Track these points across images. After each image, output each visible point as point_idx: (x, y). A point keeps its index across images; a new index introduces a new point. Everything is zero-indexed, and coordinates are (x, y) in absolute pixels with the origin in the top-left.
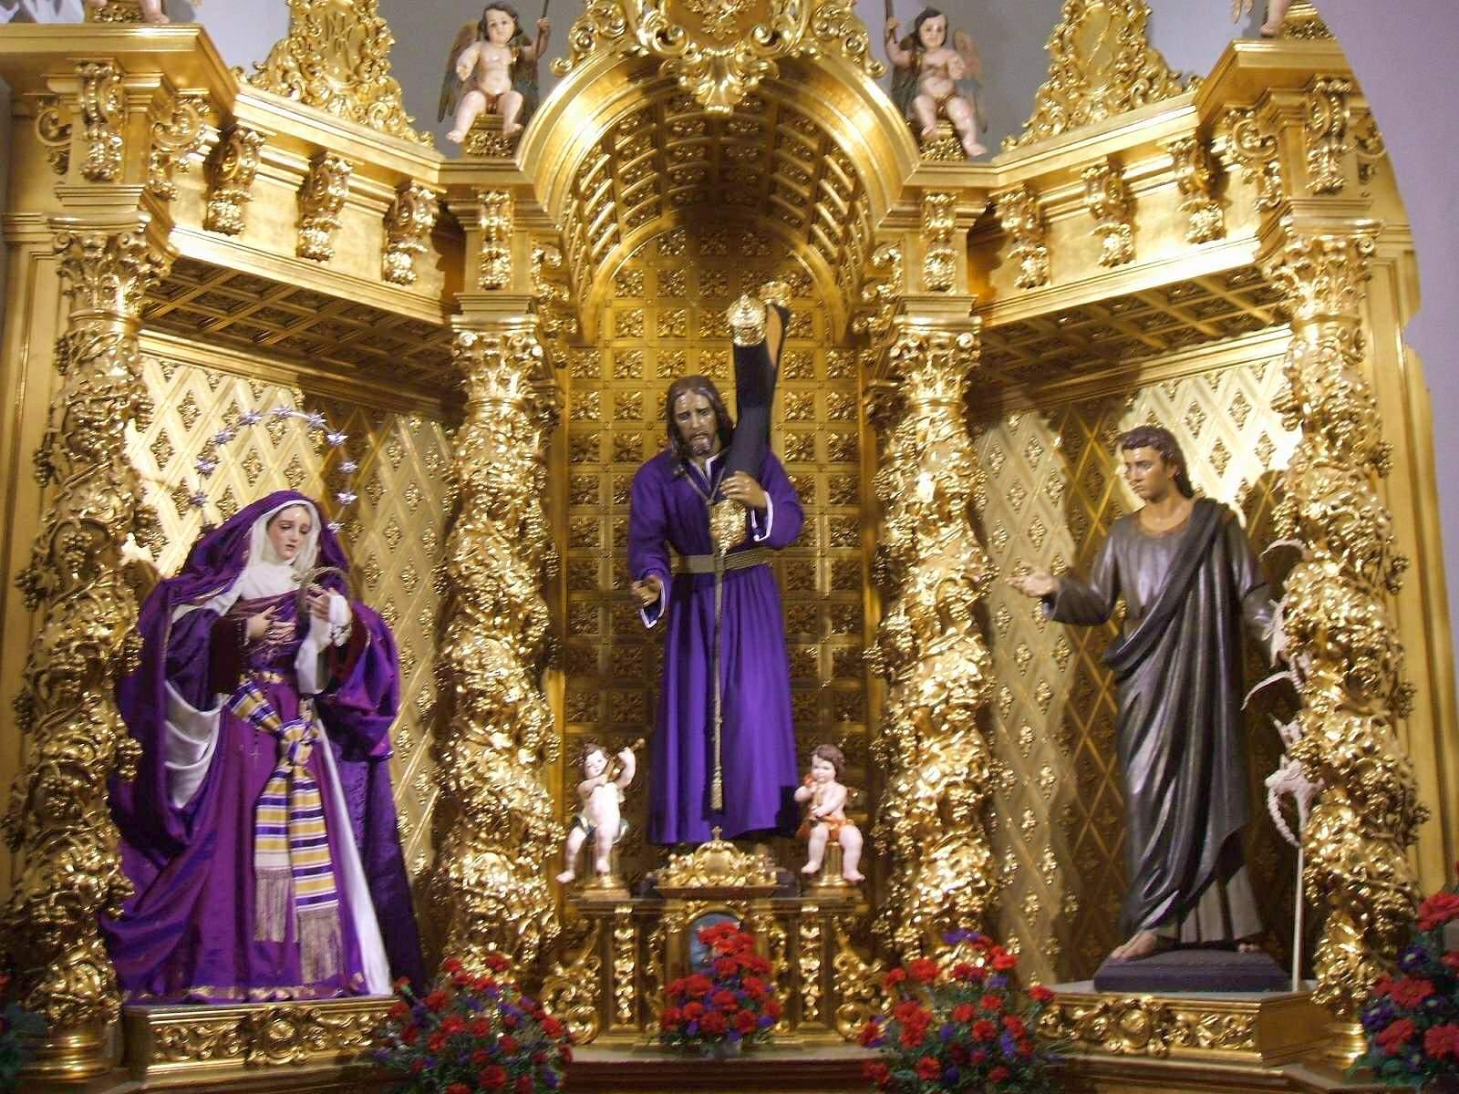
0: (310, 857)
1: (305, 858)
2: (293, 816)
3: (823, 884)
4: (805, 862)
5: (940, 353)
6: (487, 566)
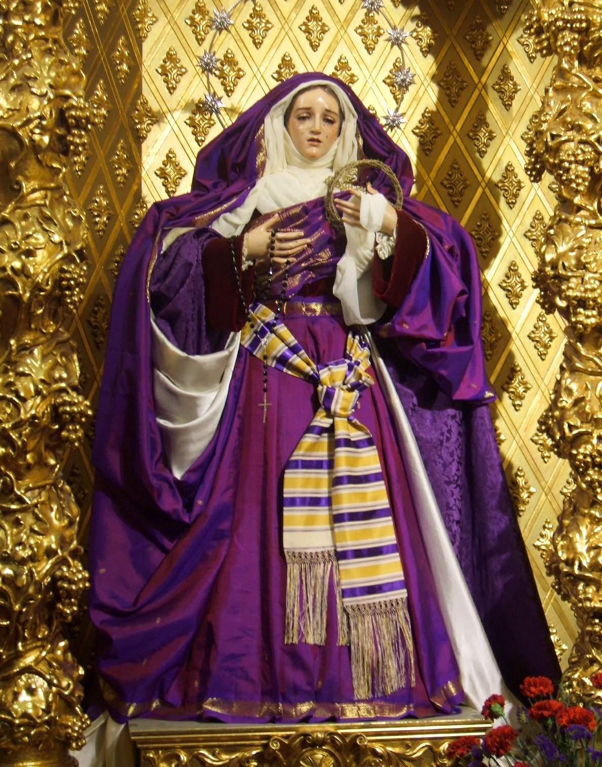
0: (367, 533)
1: (354, 535)
2: (337, 481)
6: (579, 129)
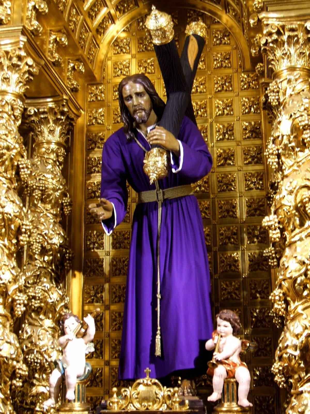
3: (224, 409)
4: (211, 391)
5: (291, 34)
